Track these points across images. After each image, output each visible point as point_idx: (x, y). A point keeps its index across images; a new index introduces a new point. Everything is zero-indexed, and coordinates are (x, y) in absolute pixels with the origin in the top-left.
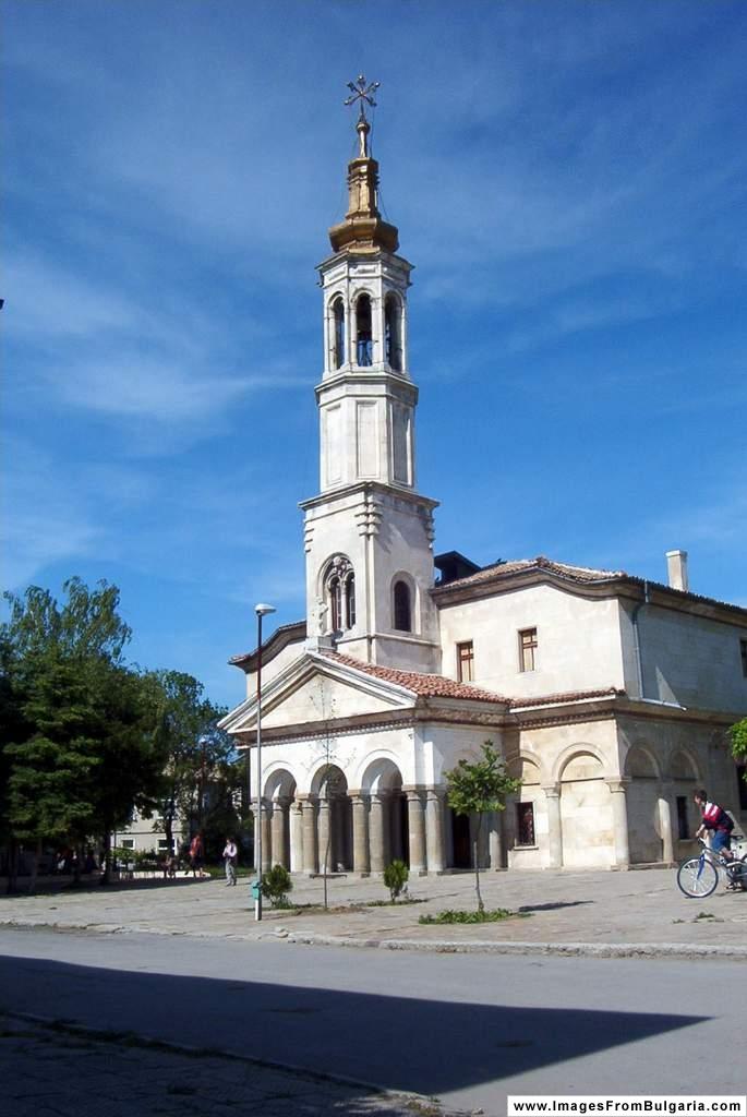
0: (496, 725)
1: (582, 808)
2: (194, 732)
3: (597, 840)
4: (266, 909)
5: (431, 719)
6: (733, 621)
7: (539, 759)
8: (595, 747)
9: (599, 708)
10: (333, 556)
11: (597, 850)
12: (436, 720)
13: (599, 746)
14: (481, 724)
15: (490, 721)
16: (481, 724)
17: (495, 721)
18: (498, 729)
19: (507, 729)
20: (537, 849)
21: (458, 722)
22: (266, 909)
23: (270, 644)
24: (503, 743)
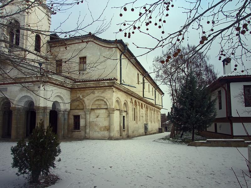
0: (69, 88)
1: (97, 118)
2: (16, 110)
3: (102, 129)
4: (246, 94)
5: (48, 82)
6: (137, 67)
7: (84, 101)
8: (105, 98)
9: (108, 85)
11: (102, 133)
12: (50, 83)
13: (106, 98)
14: (65, 87)
15: (68, 86)
16: (65, 87)
17: (69, 87)
18: (70, 90)
19: (73, 90)
20: (80, 131)
21: (57, 85)
22: (246, 94)
23: (7, 75)
24: (71, 95)
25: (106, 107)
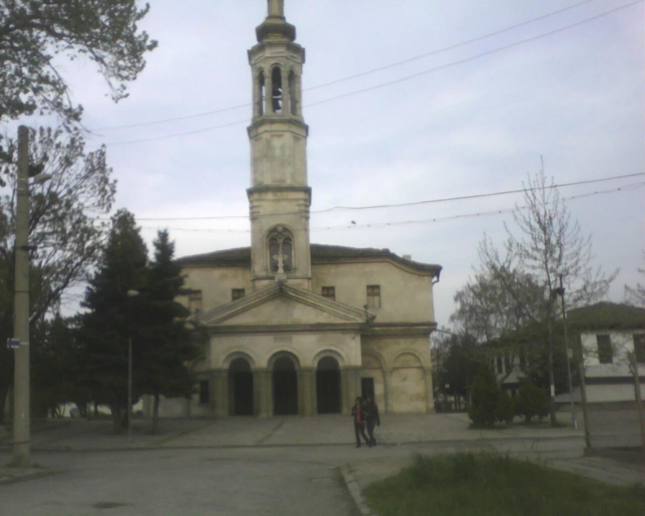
10: (278, 225)
25: (417, 365)
